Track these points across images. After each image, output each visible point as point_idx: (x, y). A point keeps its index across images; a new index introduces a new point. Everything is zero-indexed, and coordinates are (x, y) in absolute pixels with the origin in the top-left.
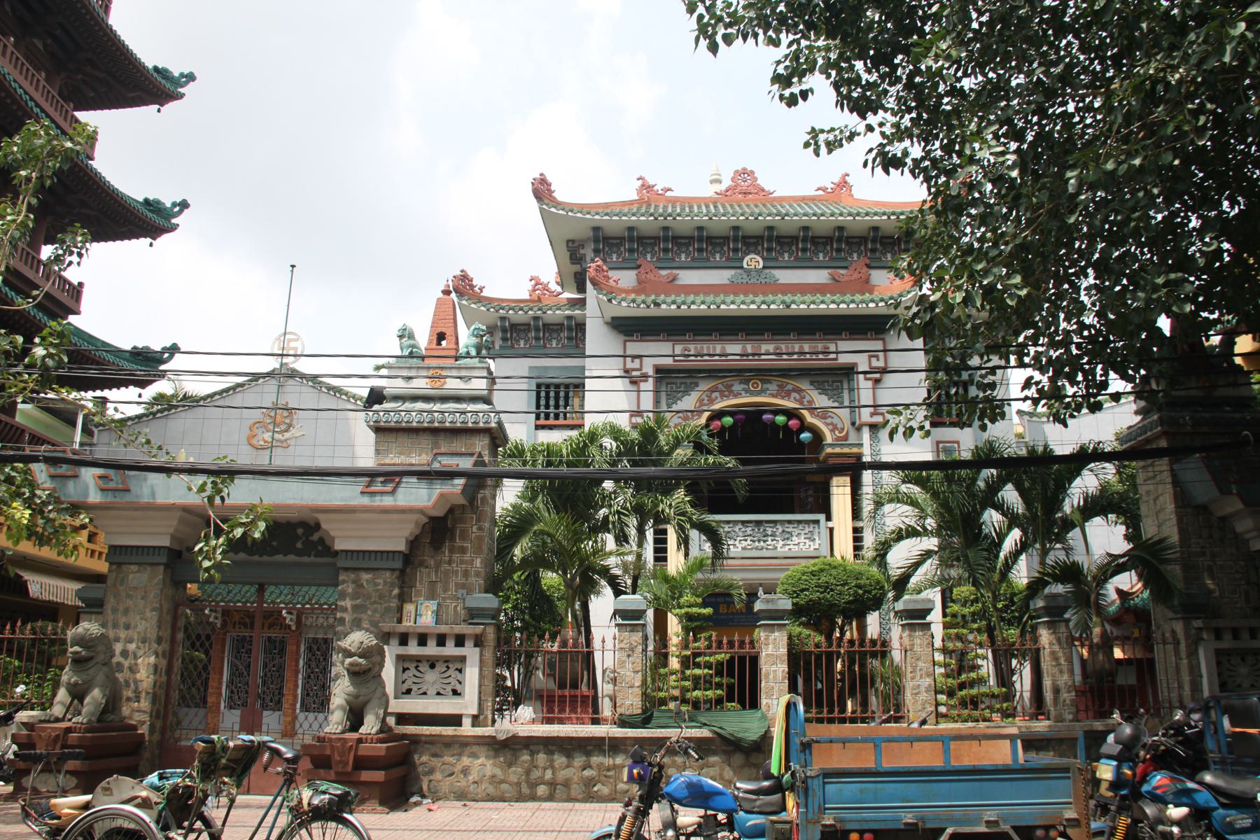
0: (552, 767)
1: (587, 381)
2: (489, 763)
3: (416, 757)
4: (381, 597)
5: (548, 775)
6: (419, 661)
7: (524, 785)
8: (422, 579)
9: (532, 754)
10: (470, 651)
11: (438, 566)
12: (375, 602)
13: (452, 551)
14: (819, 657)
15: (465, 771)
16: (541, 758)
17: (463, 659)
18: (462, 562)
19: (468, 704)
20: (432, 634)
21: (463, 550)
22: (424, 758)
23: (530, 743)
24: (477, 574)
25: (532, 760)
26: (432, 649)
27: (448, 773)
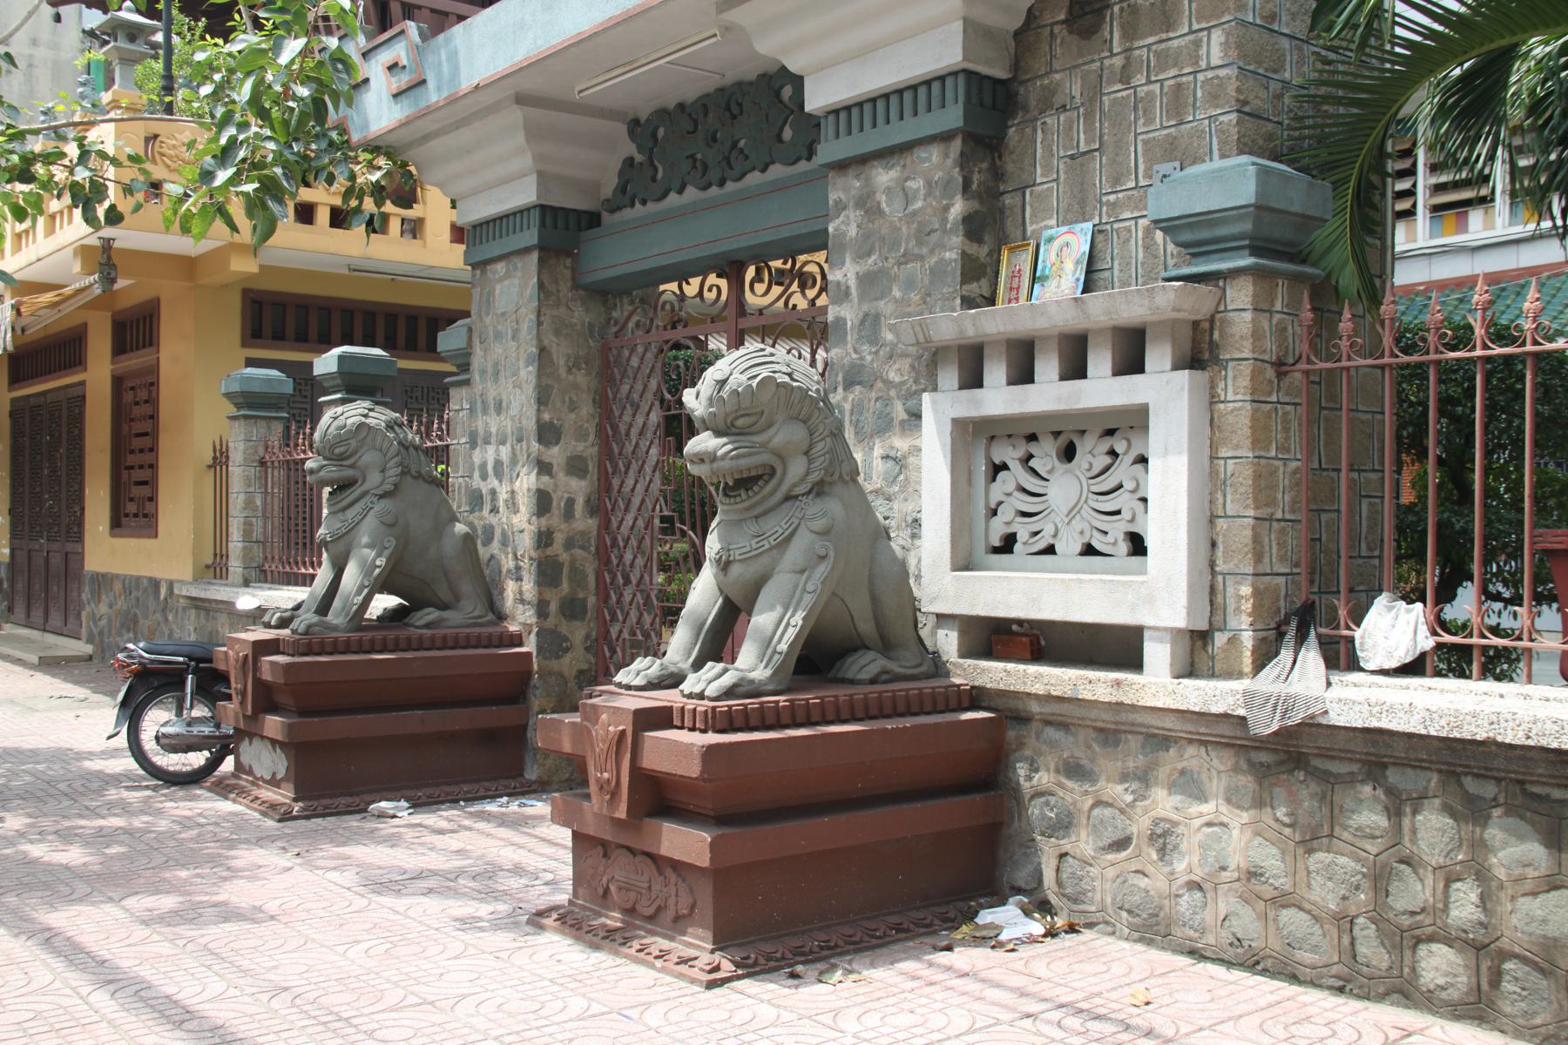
0: (1482, 876)
2: (1239, 819)
3: (1022, 770)
4: (923, 234)
5: (1464, 906)
6: (1032, 438)
7: (1366, 932)
8: (1047, 150)
9: (1398, 805)
10: (1164, 391)
11: (1094, 91)
12: (906, 258)
13: (1130, 33)
15: (1163, 839)
16: (1433, 829)
17: (1135, 420)
18: (1165, 60)
19: (1157, 596)
20: (1046, 338)
22: (1043, 778)
23: (1381, 756)
24: (1214, 98)
25: (1397, 829)
26: (1049, 394)
27: (1110, 836)
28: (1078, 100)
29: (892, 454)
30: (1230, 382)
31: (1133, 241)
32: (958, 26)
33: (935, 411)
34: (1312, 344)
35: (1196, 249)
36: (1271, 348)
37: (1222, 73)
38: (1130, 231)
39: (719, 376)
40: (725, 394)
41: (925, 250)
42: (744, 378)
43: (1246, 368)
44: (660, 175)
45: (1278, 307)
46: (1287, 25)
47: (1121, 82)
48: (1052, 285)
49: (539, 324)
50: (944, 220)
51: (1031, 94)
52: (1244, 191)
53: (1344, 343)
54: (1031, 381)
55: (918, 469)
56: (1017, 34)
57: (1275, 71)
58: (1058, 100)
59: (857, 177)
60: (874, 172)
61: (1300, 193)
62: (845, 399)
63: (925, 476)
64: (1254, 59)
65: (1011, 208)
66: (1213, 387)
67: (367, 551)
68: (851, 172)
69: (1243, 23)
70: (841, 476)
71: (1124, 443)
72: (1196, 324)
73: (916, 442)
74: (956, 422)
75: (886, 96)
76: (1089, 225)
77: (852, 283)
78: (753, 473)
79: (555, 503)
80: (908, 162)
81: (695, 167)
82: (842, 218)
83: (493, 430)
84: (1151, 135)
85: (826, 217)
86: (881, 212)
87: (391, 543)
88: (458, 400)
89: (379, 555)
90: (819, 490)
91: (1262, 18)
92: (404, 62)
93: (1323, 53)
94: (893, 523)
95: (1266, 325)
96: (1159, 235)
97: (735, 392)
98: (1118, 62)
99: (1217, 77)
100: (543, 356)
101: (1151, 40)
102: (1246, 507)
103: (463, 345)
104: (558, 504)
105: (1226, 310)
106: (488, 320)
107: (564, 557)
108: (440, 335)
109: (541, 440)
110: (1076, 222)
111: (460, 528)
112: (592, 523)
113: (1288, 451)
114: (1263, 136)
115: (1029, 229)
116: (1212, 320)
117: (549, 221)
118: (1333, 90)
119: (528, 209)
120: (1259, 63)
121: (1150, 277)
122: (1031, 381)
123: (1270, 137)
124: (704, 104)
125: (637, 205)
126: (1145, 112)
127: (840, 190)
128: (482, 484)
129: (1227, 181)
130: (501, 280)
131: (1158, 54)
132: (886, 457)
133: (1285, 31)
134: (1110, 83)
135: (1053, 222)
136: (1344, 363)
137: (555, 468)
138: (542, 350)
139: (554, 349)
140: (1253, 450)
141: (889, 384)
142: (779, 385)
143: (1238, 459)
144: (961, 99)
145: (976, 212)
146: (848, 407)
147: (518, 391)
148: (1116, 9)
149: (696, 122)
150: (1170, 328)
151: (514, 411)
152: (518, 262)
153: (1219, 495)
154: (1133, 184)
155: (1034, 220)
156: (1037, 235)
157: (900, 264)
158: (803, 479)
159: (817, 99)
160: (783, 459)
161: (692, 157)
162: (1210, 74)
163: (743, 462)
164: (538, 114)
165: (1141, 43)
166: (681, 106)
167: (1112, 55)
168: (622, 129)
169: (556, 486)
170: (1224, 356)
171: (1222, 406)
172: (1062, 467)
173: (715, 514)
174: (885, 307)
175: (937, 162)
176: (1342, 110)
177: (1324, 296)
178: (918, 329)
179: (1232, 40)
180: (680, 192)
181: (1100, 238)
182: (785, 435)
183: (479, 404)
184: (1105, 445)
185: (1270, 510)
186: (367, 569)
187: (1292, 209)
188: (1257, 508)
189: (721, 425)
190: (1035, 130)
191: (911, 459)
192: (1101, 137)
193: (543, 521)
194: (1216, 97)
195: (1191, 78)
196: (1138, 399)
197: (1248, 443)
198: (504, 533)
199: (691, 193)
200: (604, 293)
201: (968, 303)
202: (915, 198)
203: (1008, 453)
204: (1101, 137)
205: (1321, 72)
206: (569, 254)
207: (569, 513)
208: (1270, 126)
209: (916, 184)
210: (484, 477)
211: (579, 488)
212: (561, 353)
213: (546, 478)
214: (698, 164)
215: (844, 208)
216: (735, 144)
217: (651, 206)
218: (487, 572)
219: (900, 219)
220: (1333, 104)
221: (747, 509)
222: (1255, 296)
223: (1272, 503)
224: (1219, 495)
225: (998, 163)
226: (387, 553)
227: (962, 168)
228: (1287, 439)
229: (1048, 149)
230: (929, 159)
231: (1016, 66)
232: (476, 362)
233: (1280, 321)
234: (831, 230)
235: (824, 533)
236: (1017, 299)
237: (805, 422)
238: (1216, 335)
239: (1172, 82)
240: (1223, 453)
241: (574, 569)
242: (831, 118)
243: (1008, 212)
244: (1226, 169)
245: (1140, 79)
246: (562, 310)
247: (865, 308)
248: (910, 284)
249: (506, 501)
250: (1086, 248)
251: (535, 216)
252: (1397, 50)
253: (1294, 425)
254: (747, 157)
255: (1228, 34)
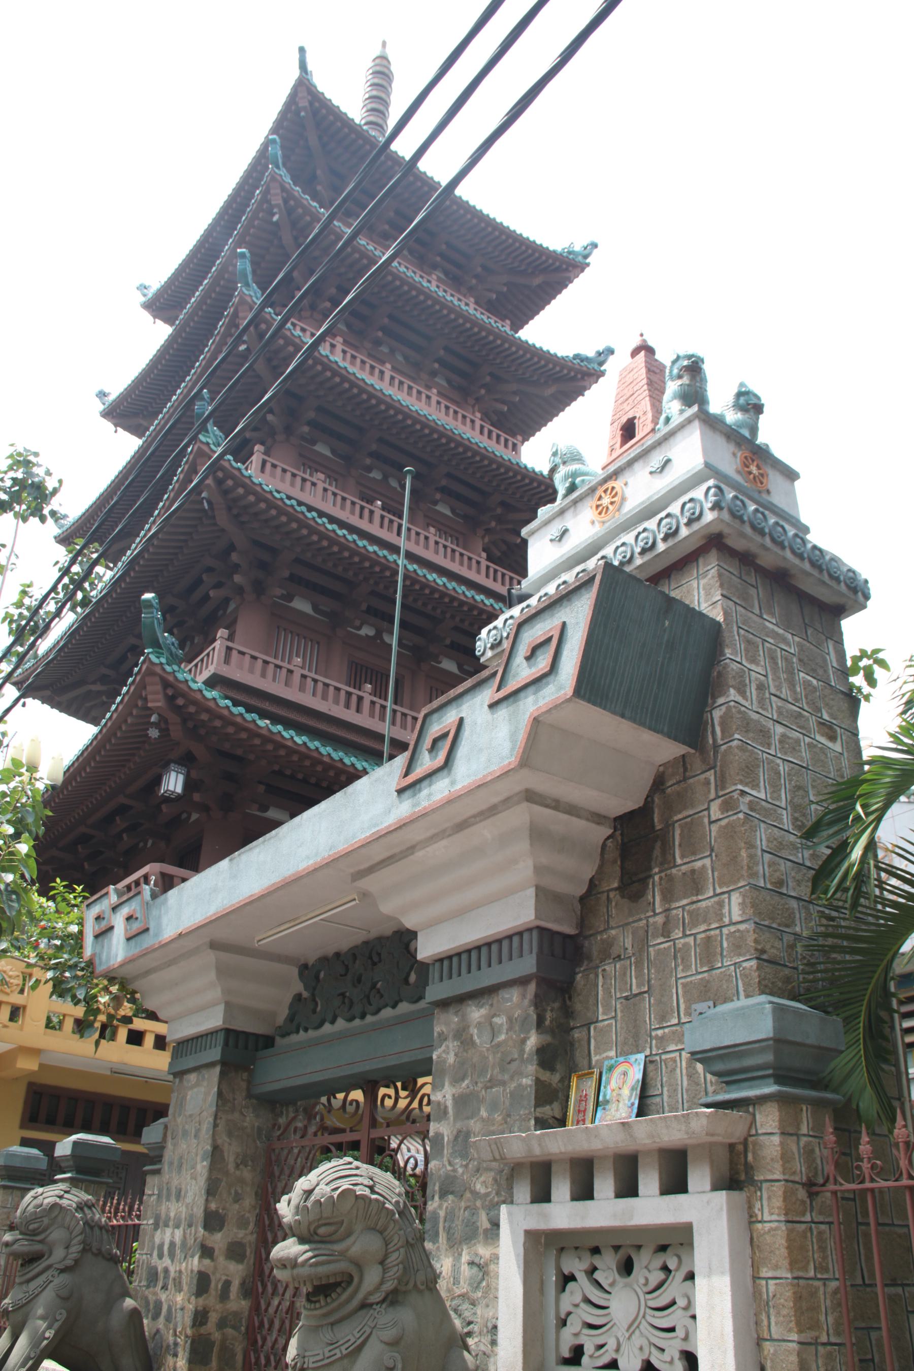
1: (423, 165)
4: (505, 1063)
6: (596, 1251)
8: (608, 993)
10: (705, 1210)
11: (643, 943)
12: (492, 1083)
13: (668, 896)
14: (168, 1199)
17: (674, 1241)
18: (696, 918)
20: (604, 1158)
21: (695, 883)
24: (737, 947)
26: (605, 1211)
28: (630, 951)
29: (477, 1260)
30: (765, 1203)
31: (678, 1070)
32: (531, 892)
33: (511, 1222)
34: (837, 1165)
35: (729, 1078)
36: (800, 1169)
37: (742, 927)
38: (675, 1061)
39: (307, 1186)
40: (309, 1204)
41: (506, 1077)
42: (328, 1189)
43: (778, 1189)
44: (319, 1008)
45: (804, 1130)
46: (794, 889)
47: (663, 936)
48: (612, 1107)
49: (215, 1125)
50: (522, 1051)
51: (593, 946)
52: (763, 1027)
53: (865, 1165)
54: (591, 1197)
55: (497, 1277)
56: (582, 899)
57: (787, 926)
58: (615, 951)
59: (456, 1013)
60: (469, 1009)
61: (814, 1028)
62: (440, 1206)
63: (502, 1284)
64: (768, 912)
65: (579, 1041)
66: (750, 1207)
67: (40, 1322)
68: (452, 1010)
69: (755, 887)
70: (415, 1285)
71: (675, 1259)
72: (732, 1146)
73: (494, 1251)
74: (528, 1233)
75: (478, 948)
76: (641, 1057)
77: (450, 1103)
78: (332, 1280)
79: (213, 1285)
80: (495, 1001)
81: (344, 1003)
82: (443, 1047)
83: (172, 1215)
84: (689, 979)
85: (431, 1047)
86: (472, 1043)
87: (62, 1316)
88: (152, 1185)
89: (49, 1327)
90: (393, 1298)
91: (772, 883)
92: (138, 915)
93: (827, 911)
94: (475, 1328)
95: (794, 1148)
96: (699, 1067)
97: (318, 1202)
98: (660, 919)
99: (738, 931)
100: (216, 1153)
101: (685, 902)
102: (790, 1330)
103: (159, 1140)
104: (215, 1286)
105: (757, 1134)
106: (179, 1120)
107: (217, 1336)
108: (145, 1130)
109: (206, 1227)
110: (631, 1053)
111: (129, 1303)
112: (245, 1304)
113: (826, 1270)
114: (777, 978)
115: (594, 1059)
116: (745, 1143)
117: (231, 1042)
118: (839, 942)
119: (217, 1032)
120: (773, 919)
121: (693, 1104)
122: (591, 1197)
123: (787, 980)
124: (354, 953)
125: (301, 1032)
126: (683, 959)
127: (445, 1023)
128: (159, 1262)
129: (748, 1018)
130: (192, 1088)
131: (690, 913)
132: (471, 1263)
133: (793, 894)
134: (655, 936)
135: (612, 1053)
136: (868, 1185)
137: (217, 1252)
138: (216, 1148)
139: (226, 1148)
140: (791, 1270)
141: (475, 1194)
142: (357, 1197)
143: (778, 1278)
144: (535, 950)
145: (549, 1045)
146: (442, 1213)
147: (194, 1182)
148: (657, 878)
149: (347, 967)
150: (708, 1149)
151: (189, 1200)
152: (206, 1073)
153: (764, 1317)
154: (675, 1021)
155: (599, 1051)
156: (600, 1064)
157: (486, 1088)
158: (378, 1288)
159: (428, 948)
160: (359, 1266)
161: (343, 995)
162: (733, 929)
163: (321, 1270)
164: (225, 956)
165: (677, 904)
166: (337, 955)
167: (655, 914)
168: (295, 971)
169: (216, 1268)
170: (759, 1177)
171: (759, 1226)
172: (621, 1281)
173: (298, 1318)
174: (474, 1125)
175: (517, 1002)
176: (848, 957)
177: (846, 1120)
178: (494, 1146)
179: (748, 901)
180: (333, 1022)
181: (651, 1067)
182: (362, 1244)
183: (165, 1192)
184: (658, 1262)
185: (814, 1334)
186: (35, 1342)
187: (809, 1041)
188: (800, 1331)
189: (305, 1232)
190: (597, 976)
191: (492, 1267)
192: (649, 981)
193: (201, 1301)
194: (739, 947)
195: (718, 931)
196: (683, 1218)
197: (785, 1263)
198: (170, 1308)
199: (341, 1023)
200: (273, 1102)
201: (542, 1123)
202: (500, 1032)
203: (575, 1265)
204: (649, 981)
205: (826, 926)
206: (246, 1069)
207: (224, 1295)
208: (787, 971)
209: (500, 1020)
210: (161, 1256)
211: (236, 1271)
212: (231, 1151)
213: (207, 1262)
214: (346, 1000)
215: (445, 1039)
216: (374, 986)
217: (311, 1033)
218: (151, 1345)
219: (488, 1050)
220: (839, 952)
221: (325, 1315)
222: (781, 1121)
223: (815, 1325)
224: (764, 1317)
225: (568, 1002)
226: (57, 1325)
227: (536, 1006)
228: (825, 1258)
229: (607, 991)
230: (510, 1000)
231: (582, 923)
232: (168, 1155)
233: (808, 1144)
234: (434, 1057)
235: (394, 1344)
236: (584, 1120)
237: (381, 1233)
238: (750, 1157)
239: (703, 935)
240: (765, 1272)
241: (224, 1348)
242: (437, 965)
243: (577, 1045)
244: (748, 1007)
245: (677, 933)
246: (236, 1115)
247: (459, 1125)
248: (494, 1106)
249: (174, 1279)
250: (640, 1076)
251: (221, 1037)
252: (888, 909)
253: (831, 1244)
254: (382, 996)
255: (744, 896)
